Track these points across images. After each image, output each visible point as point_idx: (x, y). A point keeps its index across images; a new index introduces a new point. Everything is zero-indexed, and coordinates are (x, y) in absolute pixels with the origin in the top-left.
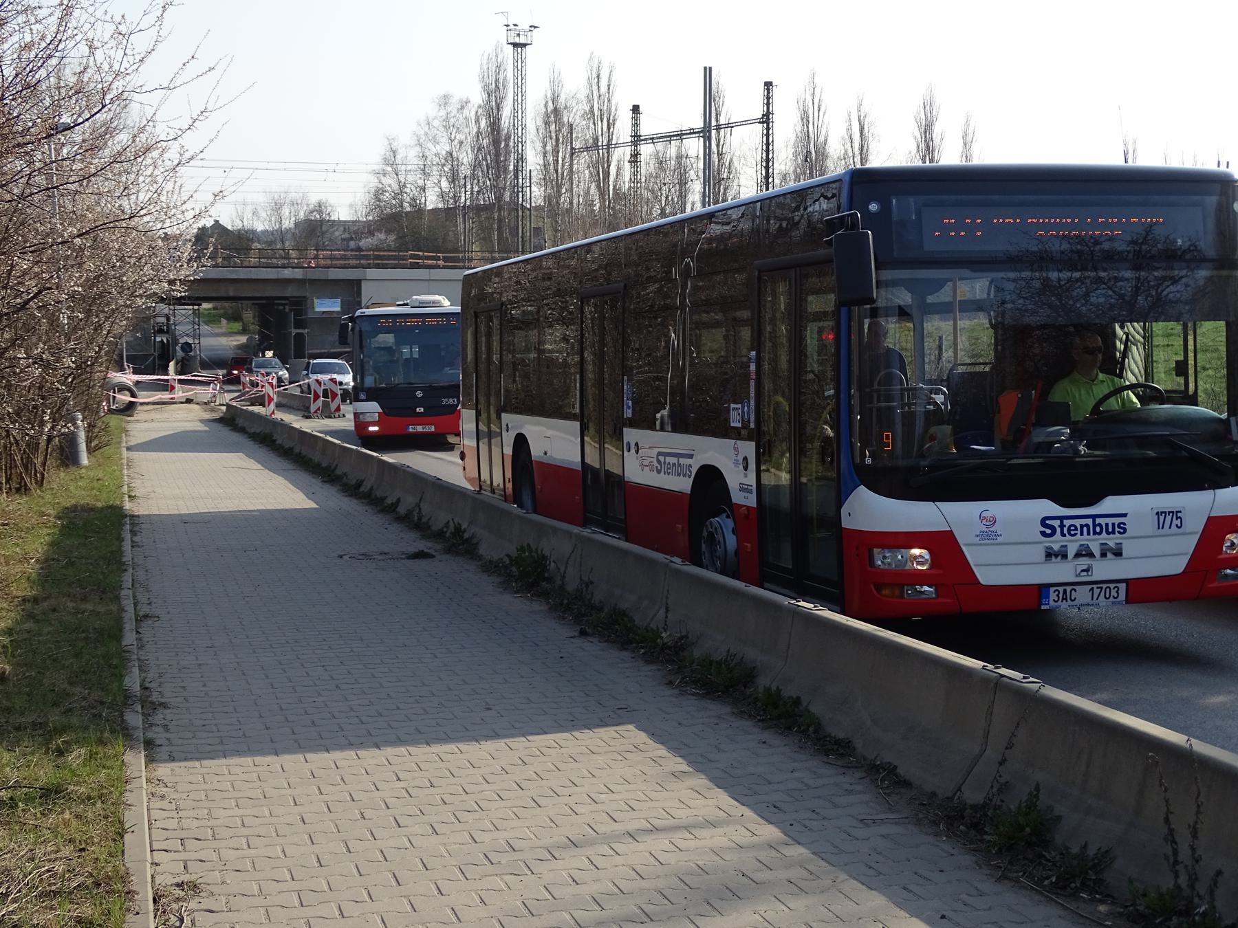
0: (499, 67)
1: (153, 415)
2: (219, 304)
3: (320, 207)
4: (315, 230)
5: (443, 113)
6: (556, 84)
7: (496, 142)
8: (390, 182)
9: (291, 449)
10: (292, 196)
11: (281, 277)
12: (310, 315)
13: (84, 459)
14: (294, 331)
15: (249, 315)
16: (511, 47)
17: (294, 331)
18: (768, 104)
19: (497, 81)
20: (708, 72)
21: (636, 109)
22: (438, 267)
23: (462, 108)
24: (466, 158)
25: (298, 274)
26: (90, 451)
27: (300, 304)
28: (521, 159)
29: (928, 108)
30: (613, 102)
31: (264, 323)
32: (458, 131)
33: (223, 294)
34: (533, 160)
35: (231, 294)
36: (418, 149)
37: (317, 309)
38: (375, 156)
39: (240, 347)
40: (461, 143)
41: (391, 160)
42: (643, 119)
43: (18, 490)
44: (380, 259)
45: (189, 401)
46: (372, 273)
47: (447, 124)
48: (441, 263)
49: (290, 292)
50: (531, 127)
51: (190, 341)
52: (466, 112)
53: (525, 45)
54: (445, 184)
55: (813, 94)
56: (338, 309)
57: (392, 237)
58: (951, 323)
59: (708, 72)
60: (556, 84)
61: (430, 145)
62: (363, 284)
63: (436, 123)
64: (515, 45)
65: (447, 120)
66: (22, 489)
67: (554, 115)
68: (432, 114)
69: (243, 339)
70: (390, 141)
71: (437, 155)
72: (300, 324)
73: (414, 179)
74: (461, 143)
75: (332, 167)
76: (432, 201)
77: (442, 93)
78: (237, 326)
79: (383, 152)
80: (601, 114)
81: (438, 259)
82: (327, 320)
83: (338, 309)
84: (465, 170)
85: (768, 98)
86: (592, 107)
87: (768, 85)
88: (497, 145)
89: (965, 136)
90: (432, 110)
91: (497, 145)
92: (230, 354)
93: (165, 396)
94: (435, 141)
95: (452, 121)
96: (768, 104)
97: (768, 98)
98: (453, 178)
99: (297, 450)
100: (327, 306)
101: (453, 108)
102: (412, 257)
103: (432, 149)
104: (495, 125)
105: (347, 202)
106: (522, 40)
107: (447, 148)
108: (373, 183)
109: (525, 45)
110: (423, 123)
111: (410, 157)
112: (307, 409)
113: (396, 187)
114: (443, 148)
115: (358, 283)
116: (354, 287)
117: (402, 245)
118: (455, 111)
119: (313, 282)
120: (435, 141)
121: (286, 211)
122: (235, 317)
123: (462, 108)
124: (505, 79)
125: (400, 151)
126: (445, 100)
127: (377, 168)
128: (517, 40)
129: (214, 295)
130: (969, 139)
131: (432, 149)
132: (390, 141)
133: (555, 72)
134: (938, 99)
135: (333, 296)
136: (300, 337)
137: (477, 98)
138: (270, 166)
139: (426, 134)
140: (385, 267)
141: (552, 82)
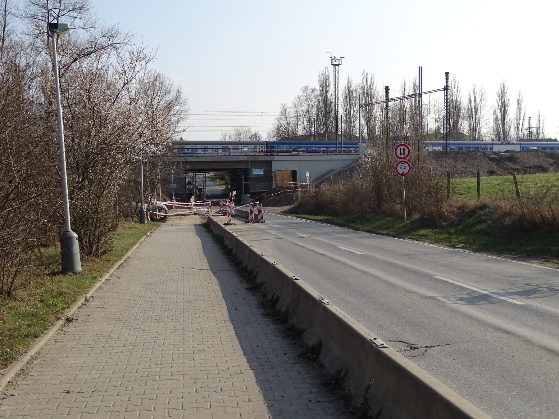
0: (326, 77)
1: (177, 222)
2: (219, 173)
3: (256, 135)
4: (254, 143)
5: (305, 94)
6: (349, 82)
7: (326, 106)
8: (283, 122)
9: (231, 250)
10: (245, 129)
12: (251, 176)
14: (244, 183)
15: (227, 178)
16: (333, 66)
17: (244, 183)
18: (447, 82)
19: (326, 82)
20: (420, 69)
21: (387, 88)
23: (313, 91)
24: (314, 112)
27: (246, 172)
28: (336, 112)
29: (502, 89)
31: (232, 180)
32: (311, 101)
33: (214, 167)
34: (341, 112)
35: (218, 167)
36: (295, 109)
37: (254, 173)
38: (278, 110)
39: (223, 190)
40: (312, 106)
41: (284, 113)
42: (390, 92)
45: (195, 214)
47: (307, 99)
49: (242, 166)
50: (341, 99)
51: (202, 187)
52: (314, 93)
53: (338, 65)
54: (305, 123)
55: (455, 85)
56: (263, 173)
58: (475, 179)
59: (420, 69)
60: (349, 82)
61: (299, 107)
62: (273, 163)
63: (302, 98)
64: (334, 65)
65: (307, 96)
67: (349, 94)
68: (300, 95)
69: (224, 187)
70: (283, 106)
71: (303, 111)
72: (246, 180)
73: (292, 121)
74: (312, 106)
75: (260, 114)
76: (301, 132)
77: (304, 86)
78: (223, 182)
80: (368, 92)
82: (258, 177)
83: (263, 173)
84: (314, 116)
85: (447, 79)
87: (447, 74)
88: (326, 107)
89: (518, 100)
90: (300, 93)
91: (326, 107)
92: (219, 193)
93: (187, 212)
94: (302, 105)
96: (447, 82)
97: (447, 79)
98: (309, 120)
99: (234, 252)
100: (258, 172)
101: (309, 92)
103: (300, 109)
104: (325, 99)
105: (266, 131)
106: (337, 63)
108: (277, 123)
109: (338, 65)
110: (297, 98)
111: (291, 111)
113: (285, 123)
114: (305, 108)
116: (269, 163)
120: (302, 105)
121: (242, 136)
122: (222, 178)
123: (313, 91)
124: (329, 81)
126: (306, 89)
127: (278, 117)
128: (335, 63)
129: (211, 168)
130: (520, 101)
131: (300, 109)
132: (283, 106)
133: (351, 76)
134: (507, 85)
136: (246, 185)
137: (318, 88)
138: (234, 114)
141: (348, 82)
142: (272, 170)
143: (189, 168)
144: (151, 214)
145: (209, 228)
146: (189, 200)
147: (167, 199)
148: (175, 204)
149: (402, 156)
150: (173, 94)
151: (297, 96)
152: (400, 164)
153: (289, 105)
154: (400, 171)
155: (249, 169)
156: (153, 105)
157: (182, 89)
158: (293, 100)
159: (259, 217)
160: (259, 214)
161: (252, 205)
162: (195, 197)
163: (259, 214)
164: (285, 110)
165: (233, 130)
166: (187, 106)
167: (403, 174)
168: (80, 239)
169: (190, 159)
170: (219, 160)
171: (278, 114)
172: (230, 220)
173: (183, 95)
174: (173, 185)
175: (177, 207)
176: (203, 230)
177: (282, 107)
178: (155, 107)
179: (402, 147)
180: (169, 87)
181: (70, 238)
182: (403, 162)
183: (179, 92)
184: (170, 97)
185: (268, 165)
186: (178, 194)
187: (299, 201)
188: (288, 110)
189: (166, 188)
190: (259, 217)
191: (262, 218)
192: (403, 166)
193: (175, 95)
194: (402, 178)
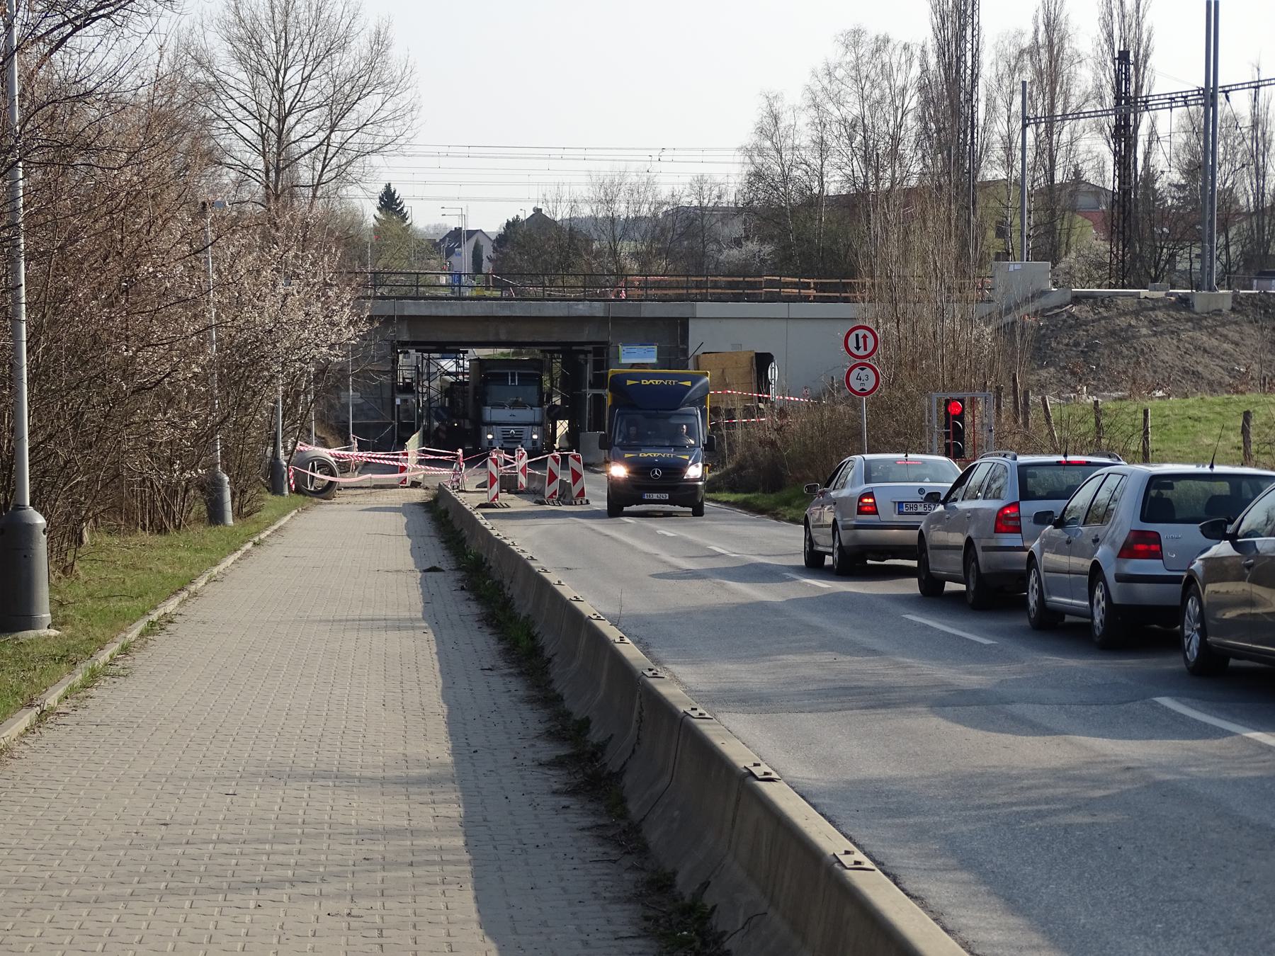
5: (850, 57)
11: (574, 313)
13: (230, 521)
22: (806, 299)
25: (598, 309)
26: (238, 514)
27: (602, 354)
30: (1145, 27)
33: (492, 338)
36: (813, 112)
41: (771, 125)
43: (159, 532)
44: (742, 286)
46: (703, 308)
48: (812, 292)
49: (586, 335)
56: (654, 360)
57: (768, 248)
61: (831, 107)
62: (692, 325)
63: (840, 73)
66: (162, 530)
68: (834, 60)
70: (771, 100)
72: (599, 381)
77: (850, 27)
79: (757, 119)
81: (807, 286)
83: (654, 360)
86: (1110, 35)
90: (835, 54)
95: (864, 70)
101: (866, 50)
102: (771, 284)
107: (856, 111)
112: (541, 493)
115: (683, 323)
116: (680, 327)
117: (784, 262)
118: (868, 54)
119: (617, 321)
125: (782, 117)
126: (856, 36)
129: (479, 339)
132: (771, 100)
135: (647, 342)
139: (824, 89)
140: (737, 298)
142: (685, 352)
143: (405, 338)
144: (297, 474)
145: (443, 522)
146: (401, 444)
147: (330, 440)
148: (355, 454)
149: (861, 352)
150: (360, 46)
151: (820, 67)
152: (857, 370)
153: (793, 98)
154: (856, 386)
155: (606, 343)
156: (282, 91)
157: (391, 34)
158: (808, 79)
159: (575, 490)
160: (575, 481)
161: (554, 457)
162: (426, 440)
163: (575, 481)
164: (776, 118)
165: (586, 179)
166: (407, 95)
167: (863, 393)
168: (233, 482)
169: (411, 309)
170: (507, 313)
171: (747, 136)
172: (497, 496)
173: (396, 54)
174: (351, 395)
175: (366, 467)
176: (423, 519)
177: (765, 104)
178: (289, 96)
179: (861, 332)
180: (345, 22)
181: (221, 480)
182: (862, 366)
183: (380, 43)
184: (345, 63)
185: (672, 336)
186: (367, 426)
187: (737, 456)
188: (786, 120)
189: (331, 407)
190: (575, 490)
191: (582, 493)
192: (863, 374)
193: (365, 52)
194: (861, 401)
